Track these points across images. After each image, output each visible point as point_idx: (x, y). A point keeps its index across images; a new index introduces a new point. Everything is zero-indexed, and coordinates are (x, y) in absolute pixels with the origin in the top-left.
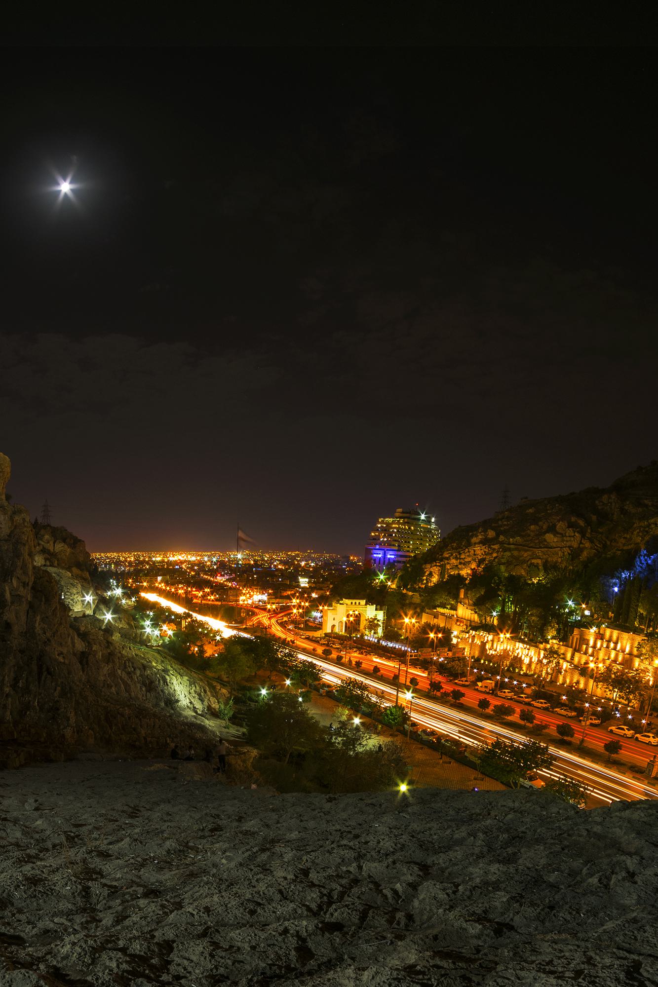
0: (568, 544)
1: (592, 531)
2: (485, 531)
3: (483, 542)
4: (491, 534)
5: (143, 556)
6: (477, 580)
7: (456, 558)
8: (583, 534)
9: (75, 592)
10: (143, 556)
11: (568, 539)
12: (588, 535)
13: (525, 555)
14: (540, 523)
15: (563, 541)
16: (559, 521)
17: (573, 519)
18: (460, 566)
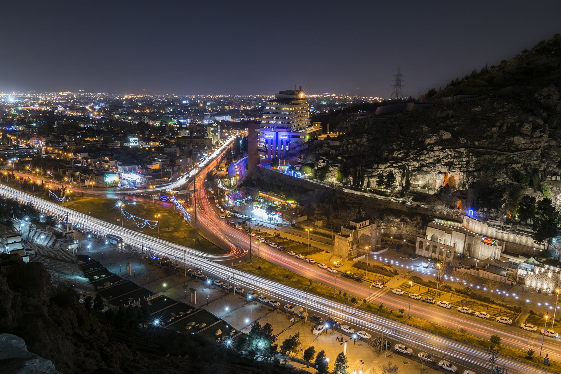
11: (537, 140)
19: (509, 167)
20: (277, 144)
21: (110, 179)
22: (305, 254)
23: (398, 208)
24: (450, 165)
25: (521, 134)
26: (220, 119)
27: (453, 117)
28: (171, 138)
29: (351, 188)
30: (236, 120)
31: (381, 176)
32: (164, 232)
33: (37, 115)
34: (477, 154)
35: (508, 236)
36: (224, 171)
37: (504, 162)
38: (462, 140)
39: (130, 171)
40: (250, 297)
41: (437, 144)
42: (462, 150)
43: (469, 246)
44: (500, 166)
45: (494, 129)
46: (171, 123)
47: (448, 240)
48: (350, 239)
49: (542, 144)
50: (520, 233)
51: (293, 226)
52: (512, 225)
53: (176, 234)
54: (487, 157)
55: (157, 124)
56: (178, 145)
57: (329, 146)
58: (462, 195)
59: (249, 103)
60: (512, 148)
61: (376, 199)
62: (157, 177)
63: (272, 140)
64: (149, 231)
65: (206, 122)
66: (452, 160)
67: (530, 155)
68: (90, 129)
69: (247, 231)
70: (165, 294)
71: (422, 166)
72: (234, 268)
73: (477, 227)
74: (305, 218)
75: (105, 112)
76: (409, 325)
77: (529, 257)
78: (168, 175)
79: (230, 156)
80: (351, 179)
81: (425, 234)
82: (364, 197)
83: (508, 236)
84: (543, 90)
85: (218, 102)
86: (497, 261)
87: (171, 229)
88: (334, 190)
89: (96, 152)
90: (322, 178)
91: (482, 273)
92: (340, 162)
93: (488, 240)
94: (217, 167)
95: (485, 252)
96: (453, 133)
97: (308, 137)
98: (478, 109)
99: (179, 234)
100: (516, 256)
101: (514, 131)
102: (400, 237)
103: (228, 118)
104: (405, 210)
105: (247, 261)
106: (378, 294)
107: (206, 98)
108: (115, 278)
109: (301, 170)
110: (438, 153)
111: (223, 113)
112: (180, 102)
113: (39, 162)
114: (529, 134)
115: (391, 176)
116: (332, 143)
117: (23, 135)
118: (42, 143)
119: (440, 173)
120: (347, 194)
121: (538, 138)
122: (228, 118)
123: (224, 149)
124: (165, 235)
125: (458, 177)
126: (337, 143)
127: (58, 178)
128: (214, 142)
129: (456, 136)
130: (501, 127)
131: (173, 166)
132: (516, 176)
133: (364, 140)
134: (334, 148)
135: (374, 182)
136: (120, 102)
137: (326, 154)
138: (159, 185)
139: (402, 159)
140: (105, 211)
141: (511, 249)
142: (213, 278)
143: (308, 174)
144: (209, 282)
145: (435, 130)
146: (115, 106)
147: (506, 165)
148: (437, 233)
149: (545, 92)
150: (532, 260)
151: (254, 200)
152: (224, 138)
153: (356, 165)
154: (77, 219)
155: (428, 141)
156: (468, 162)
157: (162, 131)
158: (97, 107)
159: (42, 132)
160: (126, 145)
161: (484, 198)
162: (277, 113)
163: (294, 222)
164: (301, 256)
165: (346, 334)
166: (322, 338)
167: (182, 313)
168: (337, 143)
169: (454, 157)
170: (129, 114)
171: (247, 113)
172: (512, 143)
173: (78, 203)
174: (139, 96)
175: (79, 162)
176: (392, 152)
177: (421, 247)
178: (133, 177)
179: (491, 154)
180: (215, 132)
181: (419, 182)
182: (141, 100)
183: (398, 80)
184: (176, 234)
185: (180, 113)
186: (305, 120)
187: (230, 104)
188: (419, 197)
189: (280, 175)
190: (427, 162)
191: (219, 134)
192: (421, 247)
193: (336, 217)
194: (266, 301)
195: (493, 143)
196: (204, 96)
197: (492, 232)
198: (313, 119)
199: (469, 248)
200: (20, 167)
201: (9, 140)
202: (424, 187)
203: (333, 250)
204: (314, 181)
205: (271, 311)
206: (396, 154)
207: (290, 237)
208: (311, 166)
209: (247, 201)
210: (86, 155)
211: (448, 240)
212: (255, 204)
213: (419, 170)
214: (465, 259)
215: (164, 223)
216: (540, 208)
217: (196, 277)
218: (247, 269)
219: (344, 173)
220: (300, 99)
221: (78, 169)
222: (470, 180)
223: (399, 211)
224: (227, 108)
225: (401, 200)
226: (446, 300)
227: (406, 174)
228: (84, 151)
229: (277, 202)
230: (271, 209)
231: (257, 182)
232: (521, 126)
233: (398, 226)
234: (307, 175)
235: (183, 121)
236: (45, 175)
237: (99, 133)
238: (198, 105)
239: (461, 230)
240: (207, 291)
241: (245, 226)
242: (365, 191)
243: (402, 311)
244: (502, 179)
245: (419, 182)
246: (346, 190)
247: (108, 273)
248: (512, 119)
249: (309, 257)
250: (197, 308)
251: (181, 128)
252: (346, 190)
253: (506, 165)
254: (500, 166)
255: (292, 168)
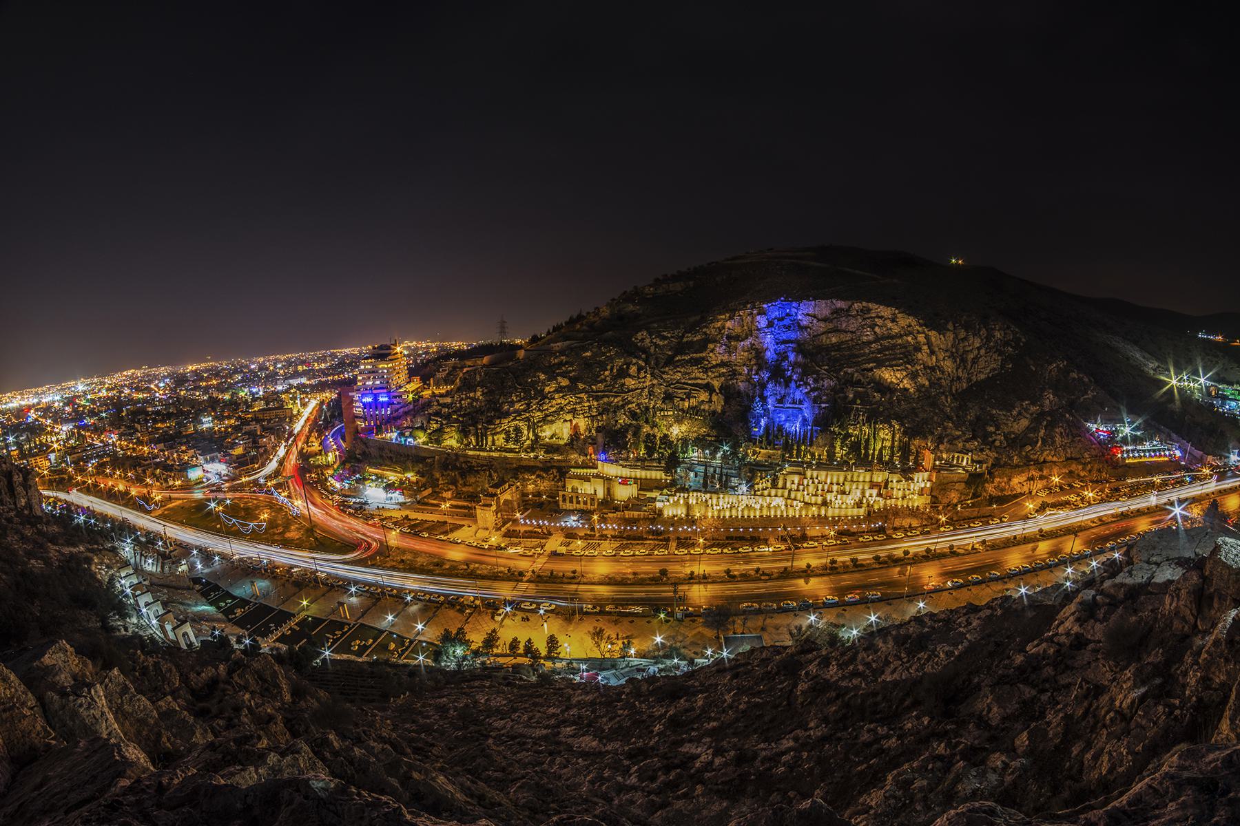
21: (194, 474)
22: (446, 533)
23: (532, 464)
24: (573, 412)
25: (630, 376)
26: (295, 382)
27: (567, 363)
28: (247, 412)
29: (474, 449)
30: (313, 382)
31: (508, 433)
32: (274, 535)
33: (105, 402)
34: (597, 398)
35: (640, 473)
36: (316, 446)
38: (581, 386)
39: (213, 460)
40: (409, 598)
41: (557, 391)
42: (582, 395)
43: (609, 490)
44: (618, 408)
45: (607, 373)
46: (242, 394)
47: (587, 488)
48: (494, 508)
49: (648, 383)
50: (648, 468)
51: (419, 502)
52: (641, 463)
53: (288, 535)
54: (606, 400)
55: (227, 397)
56: (257, 420)
57: (439, 404)
58: (594, 442)
59: (323, 359)
60: (623, 390)
61: (506, 458)
62: (243, 464)
64: (256, 537)
65: (279, 388)
67: (640, 394)
68: (158, 413)
69: (368, 517)
70: (308, 613)
71: (546, 416)
72: (373, 566)
73: (611, 470)
74: (430, 491)
75: (171, 389)
76: (585, 584)
77: (662, 489)
78: (254, 460)
79: (319, 426)
80: (473, 439)
81: (564, 486)
82: (492, 458)
83: (640, 473)
85: (290, 363)
86: (637, 499)
87: (281, 530)
88: (456, 455)
89: (170, 440)
90: (438, 441)
91: (627, 514)
92: (457, 421)
93: (625, 481)
94: (307, 442)
95: (623, 493)
96: (570, 379)
97: (411, 396)
98: (588, 354)
99: (293, 534)
100: (651, 490)
101: (623, 373)
102: (539, 494)
103: (304, 380)
104: (539, 464)
105: (381, 557)
106: (542, 560)
107: (276, 361)
108: (243, 602)
109: (411, 436)
110: (559, 400)
111: (297, 375)
112: (247, 367)
113: (119, 462)
115: (517, 430)
116: (441, 400)
117: (97, 430)
118: (114, 437)
119: (565, 421)
120: (473, 457)
122: (304, 380)
123: (308, 419)
124: (276, 537)
125: (582, 423)
126: (449, 400)
127: (139, 480)
128: (295, 412)
129: (574, 381)
130: (612, 370)
131: (258, 448)
132: (633, 415)
133: (479, 394)
134: (445, 405)
135: (500, 440)
136: (184, 375)
137: (437, 414)
138: (248, 473)
139: (525, 411)
140: (198, 516)
141: (646, 485)
142: (356, 582)
143: (422, 438)
144: (353, 589)
145: (552, 378)
146: (180, 380)
147: (623, 406)
148: (576, 483)
149: (639, 336)
150: (665, 491)
151: (365, 479)
152: (304, 405)
153: (475, 422)
154: (176, 532)
155: (547, 389)
156: (590, 407)
157: (234, 404)
158: (162, 385)
159: (116, 422)
160: (199, 427)
161: (613, 440)
163: (419, 497)
164: (443, 537)
165: (529, 611)
166: (507, 622)
167: (339, 633)
168: (449, 400)
169: (576, 403)
170: (195, 389)
171: (323, 372)
172: (624, 384)
173: (169, 509)
174: (203, 365)
175: (157, 457)
176: (512, 403)
177: (564, 500)
178: (216, 469)
179: (608, 396)
180: (294, 399)
181: (547, 432)
182: (206, 370)
183: (503, 327)
184: (288, 535)
185: (250, 380)
186: (402, 377)
187: (303, 363)
188: (551, 449)
189: (385, 446)
191: (298, 401)
192: (564, 500)
193: (465, 485)
194: (427, 597)
196: (272, 358)
197: (626, 472)
198: (412, 373)
199: (608, 491)
200: (100, 468)
201: (84, 437)
202: (551, 438)
203: (476, 521)
204: (431, 446)
205: (438, 608)
206: (517, 406)
207: (420, 516)
208: (422, 428)
209: (357, 481)
210: (161, 446)
211: (587, 488)
212: (367, 483)
213: (544, 420)
214: (608, 504)
215: (272, 524)
216: (662, 443)
217: (338, 586)
218: (388, 565)
219: (464, 433)
221: (157, 465)
222: (595, 424)
223: (533, 467)
224: (300, 368)
225: (532, 455)
226: (608, 547)
227: (532, 427)
228: (157, 441)
229: (393, 477)
230: (389, 487)
231: (361, 457)
232: (628, 368)
233: (534, 482)
234: (420, 441)
235: (254, 390)
236: (126, 477)
237: (169, 416)
238: (267, 369)
239: (597, 476)
240: (354, 600)
241: (361, 511)
242: (491, 450)
243: (574, 572)
244: (623, 419)
245: (547, 432)
246: (471, 453)
247: (234, 598)
248: (619, 362)
249: (451, 536)
250: (352, 623)
251: (254, 400)
252: (471, 453)
253: (623, 406)
254: (618, 408)
255: (401, 434)
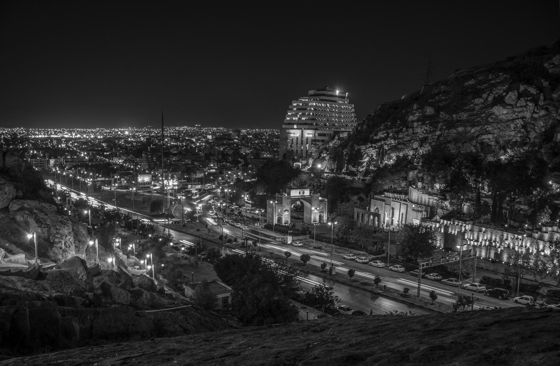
0: (520, 115)
1: (545, 99)
2: (421, 107)
3: (423, 120)
4: (429, 111)
5: (20, 131)
6: (427, 160)
7: (394, 138)
8: (535, 101)
9: (66, 232)
10: (20, 131)
11: (520, 109)
12: (541, 103)
13: (473, 131)
14: (485, 96)
15: (514, 112)
16: (507, 92)
17: (522, 88)
18: (399, 147)
19: (480, 138)
20: (302, 144)
37: (477, 133)
63: (297, 138)
66: (426, 135)
84: (554, 59)
114: (513, 103)
121: (521, 107)
162: (302, 109)
190: (405, 140)
195: (472, 116)
220: (336, 96)
